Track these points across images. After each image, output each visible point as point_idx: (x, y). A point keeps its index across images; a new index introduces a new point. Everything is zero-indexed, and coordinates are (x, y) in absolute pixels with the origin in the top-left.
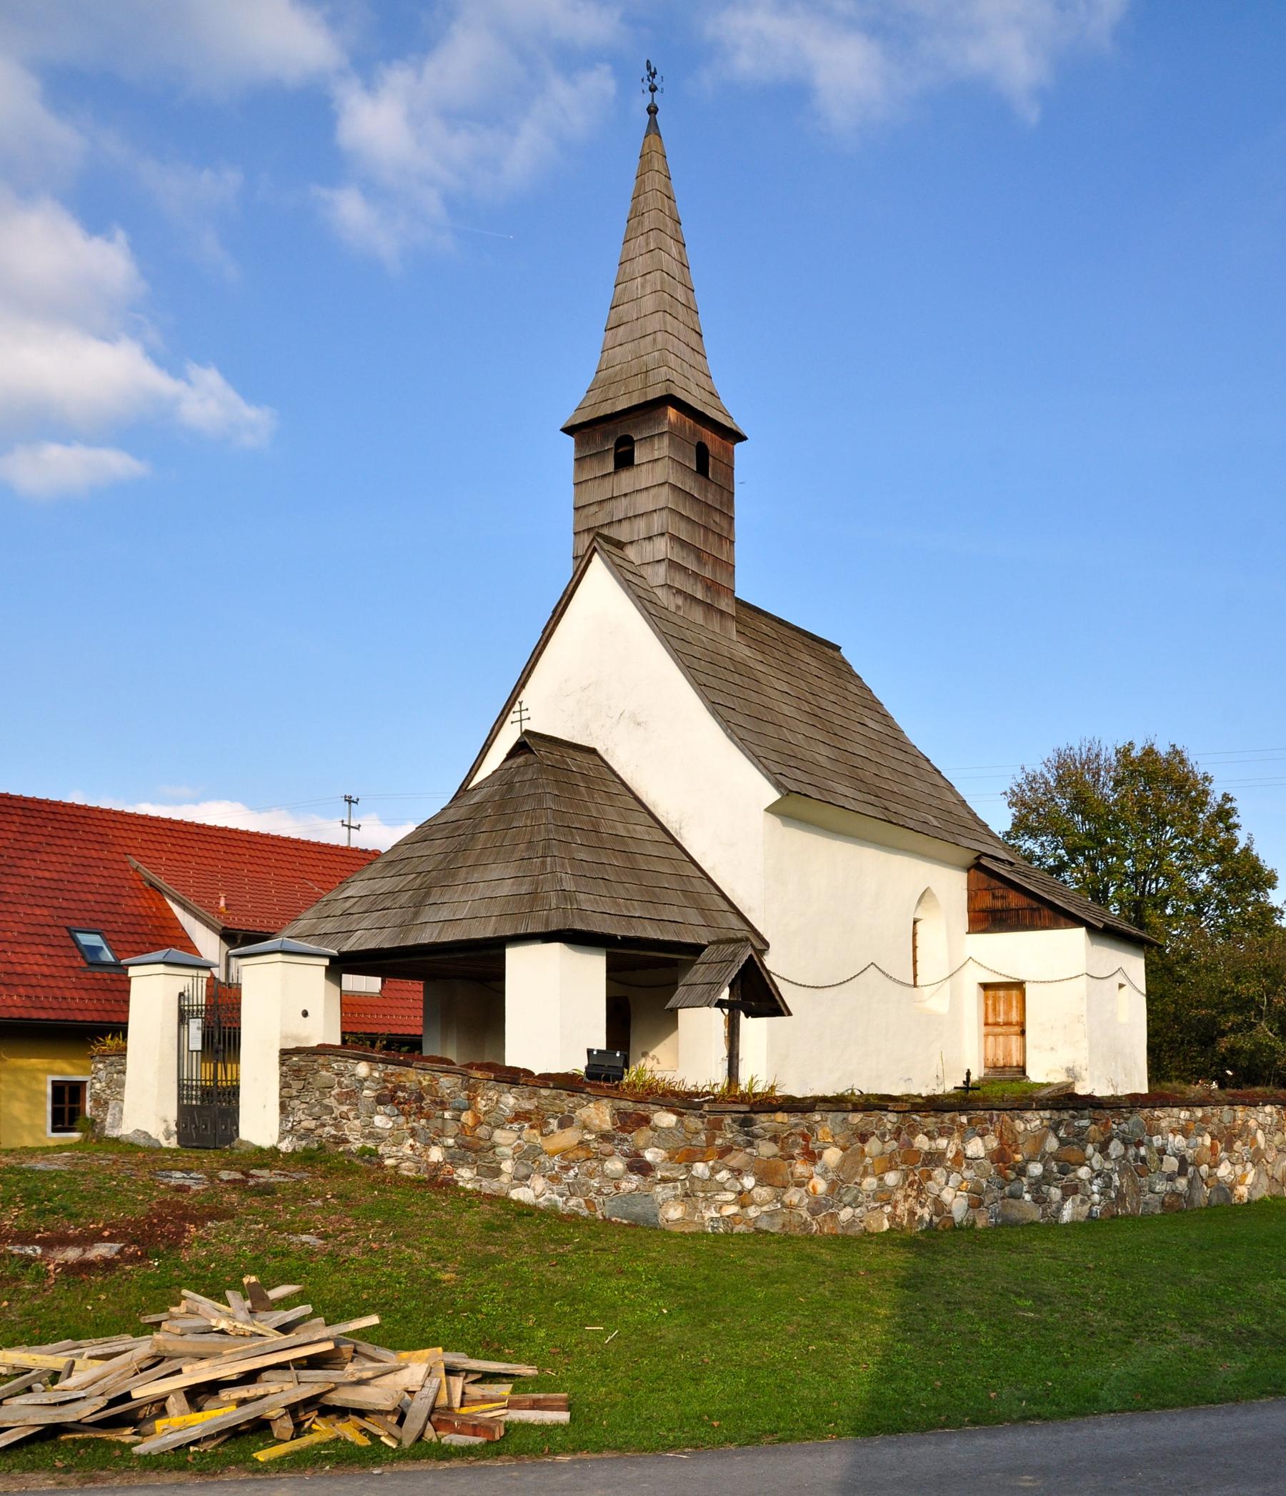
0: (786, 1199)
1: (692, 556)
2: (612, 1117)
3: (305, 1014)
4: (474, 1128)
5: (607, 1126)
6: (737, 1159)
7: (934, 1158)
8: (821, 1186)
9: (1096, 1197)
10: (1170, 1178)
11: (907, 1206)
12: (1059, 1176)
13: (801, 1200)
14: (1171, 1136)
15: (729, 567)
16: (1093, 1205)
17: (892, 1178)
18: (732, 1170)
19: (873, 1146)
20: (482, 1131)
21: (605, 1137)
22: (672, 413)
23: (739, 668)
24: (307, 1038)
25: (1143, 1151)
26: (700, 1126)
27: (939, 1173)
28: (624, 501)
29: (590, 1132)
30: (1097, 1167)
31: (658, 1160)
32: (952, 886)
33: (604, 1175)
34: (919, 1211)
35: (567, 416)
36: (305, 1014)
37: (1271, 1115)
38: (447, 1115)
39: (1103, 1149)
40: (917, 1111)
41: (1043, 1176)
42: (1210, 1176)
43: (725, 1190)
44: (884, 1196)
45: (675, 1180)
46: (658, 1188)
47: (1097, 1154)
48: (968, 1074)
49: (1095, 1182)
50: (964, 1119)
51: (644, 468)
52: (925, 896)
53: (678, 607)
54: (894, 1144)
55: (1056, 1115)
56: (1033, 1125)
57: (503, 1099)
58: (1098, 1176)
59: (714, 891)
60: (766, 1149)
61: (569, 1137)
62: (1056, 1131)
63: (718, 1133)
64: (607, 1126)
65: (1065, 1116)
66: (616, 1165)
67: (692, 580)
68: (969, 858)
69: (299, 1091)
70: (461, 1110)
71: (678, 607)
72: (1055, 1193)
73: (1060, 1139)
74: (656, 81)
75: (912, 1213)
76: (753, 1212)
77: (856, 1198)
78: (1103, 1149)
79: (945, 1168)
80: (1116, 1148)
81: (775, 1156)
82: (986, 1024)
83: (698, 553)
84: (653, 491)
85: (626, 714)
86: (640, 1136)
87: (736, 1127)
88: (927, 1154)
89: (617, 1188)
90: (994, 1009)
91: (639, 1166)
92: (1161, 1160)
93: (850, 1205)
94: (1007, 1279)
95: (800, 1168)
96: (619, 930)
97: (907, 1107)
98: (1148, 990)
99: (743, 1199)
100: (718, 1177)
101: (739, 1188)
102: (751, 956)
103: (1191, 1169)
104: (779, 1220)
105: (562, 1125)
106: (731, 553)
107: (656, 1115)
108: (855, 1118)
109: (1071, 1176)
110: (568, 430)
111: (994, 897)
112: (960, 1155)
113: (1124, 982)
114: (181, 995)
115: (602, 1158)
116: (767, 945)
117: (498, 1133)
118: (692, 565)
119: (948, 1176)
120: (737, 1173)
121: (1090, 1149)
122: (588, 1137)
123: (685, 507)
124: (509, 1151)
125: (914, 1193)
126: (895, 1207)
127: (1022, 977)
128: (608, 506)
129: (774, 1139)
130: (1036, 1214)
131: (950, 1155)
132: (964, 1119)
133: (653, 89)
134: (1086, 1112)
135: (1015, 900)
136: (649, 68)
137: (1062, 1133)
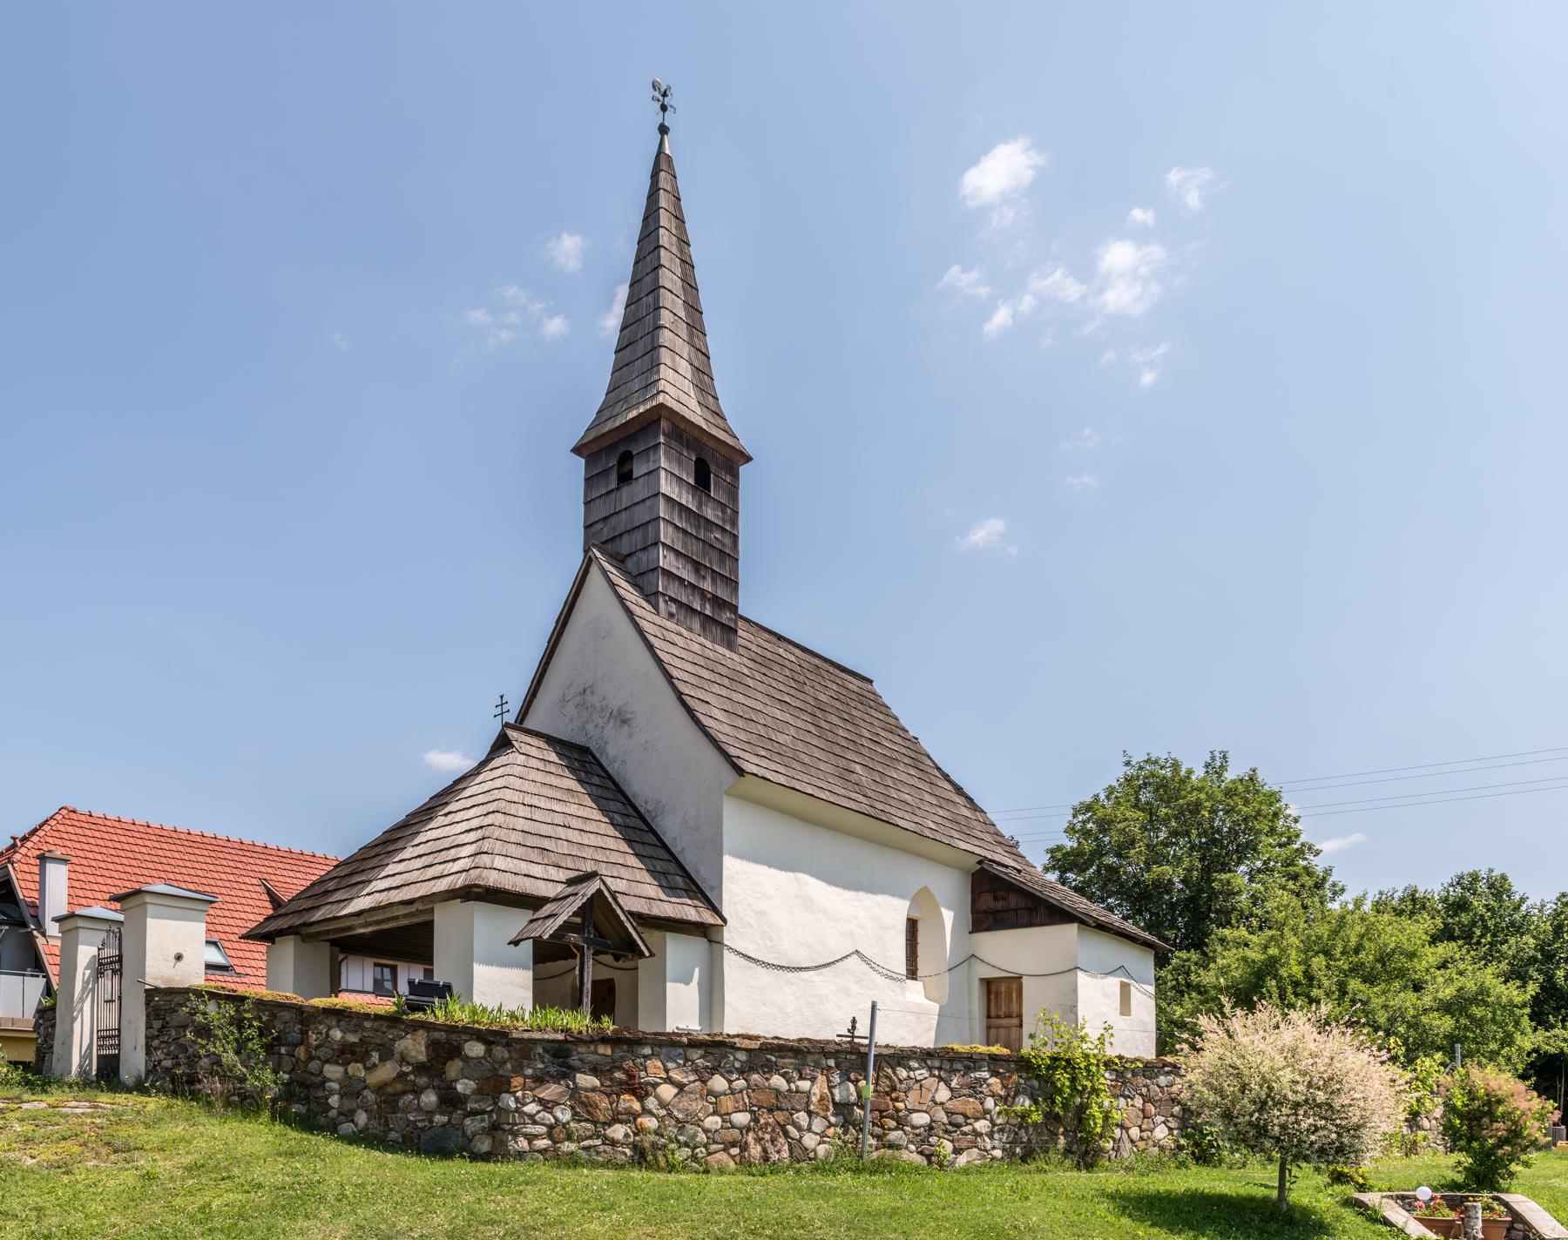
1: (689, 567)
2: (427, 1047)
3: (179, 957)
4: (306, 1063)
5: (423, 1058)
13: (627, 1135)
15: (733, 584)
18: (541, 1101)
20: (314, 1066)
26: (507, 1055)
28: (624, 515)
29: (408, 1064)
31: (468, 1092)
33: (419, 1109)
36: (179, 957)
38: (283, 1050)
42: (1142, 1139)
43: (535, 1123)
45: (483, 1112)
46: (468, 1121)
48: (854, 1021)
57: (332, 1033)
61: (386, 1072)
63: (526, 1062)
64: (423, 1058)
66: (429, 1098)
69: (160, 1030)
70: (296, 1045)
82: (989, 1017)
83: (697, 566)
84: (648, 503)
87: (547, 1057)
89: (431, 1121)
91: (451, 1100)
93: (686, 1145)
100: (526, 1109)
105: (382, 1059)
106: (735, 570)
107: (467, 1046)
110: (577, 450)
111: (996, 899)
115: (417, 1092)
116: (725, 921)
117: (327, 1067)
118: (686, 574)
120: (547, 1105)
122: (405, 1069)
124: (335, 1086)
125: (768, 1137)
127: (1021, 971)
128: (614, 520)
135: (1013, 901)
136: (655, 86)
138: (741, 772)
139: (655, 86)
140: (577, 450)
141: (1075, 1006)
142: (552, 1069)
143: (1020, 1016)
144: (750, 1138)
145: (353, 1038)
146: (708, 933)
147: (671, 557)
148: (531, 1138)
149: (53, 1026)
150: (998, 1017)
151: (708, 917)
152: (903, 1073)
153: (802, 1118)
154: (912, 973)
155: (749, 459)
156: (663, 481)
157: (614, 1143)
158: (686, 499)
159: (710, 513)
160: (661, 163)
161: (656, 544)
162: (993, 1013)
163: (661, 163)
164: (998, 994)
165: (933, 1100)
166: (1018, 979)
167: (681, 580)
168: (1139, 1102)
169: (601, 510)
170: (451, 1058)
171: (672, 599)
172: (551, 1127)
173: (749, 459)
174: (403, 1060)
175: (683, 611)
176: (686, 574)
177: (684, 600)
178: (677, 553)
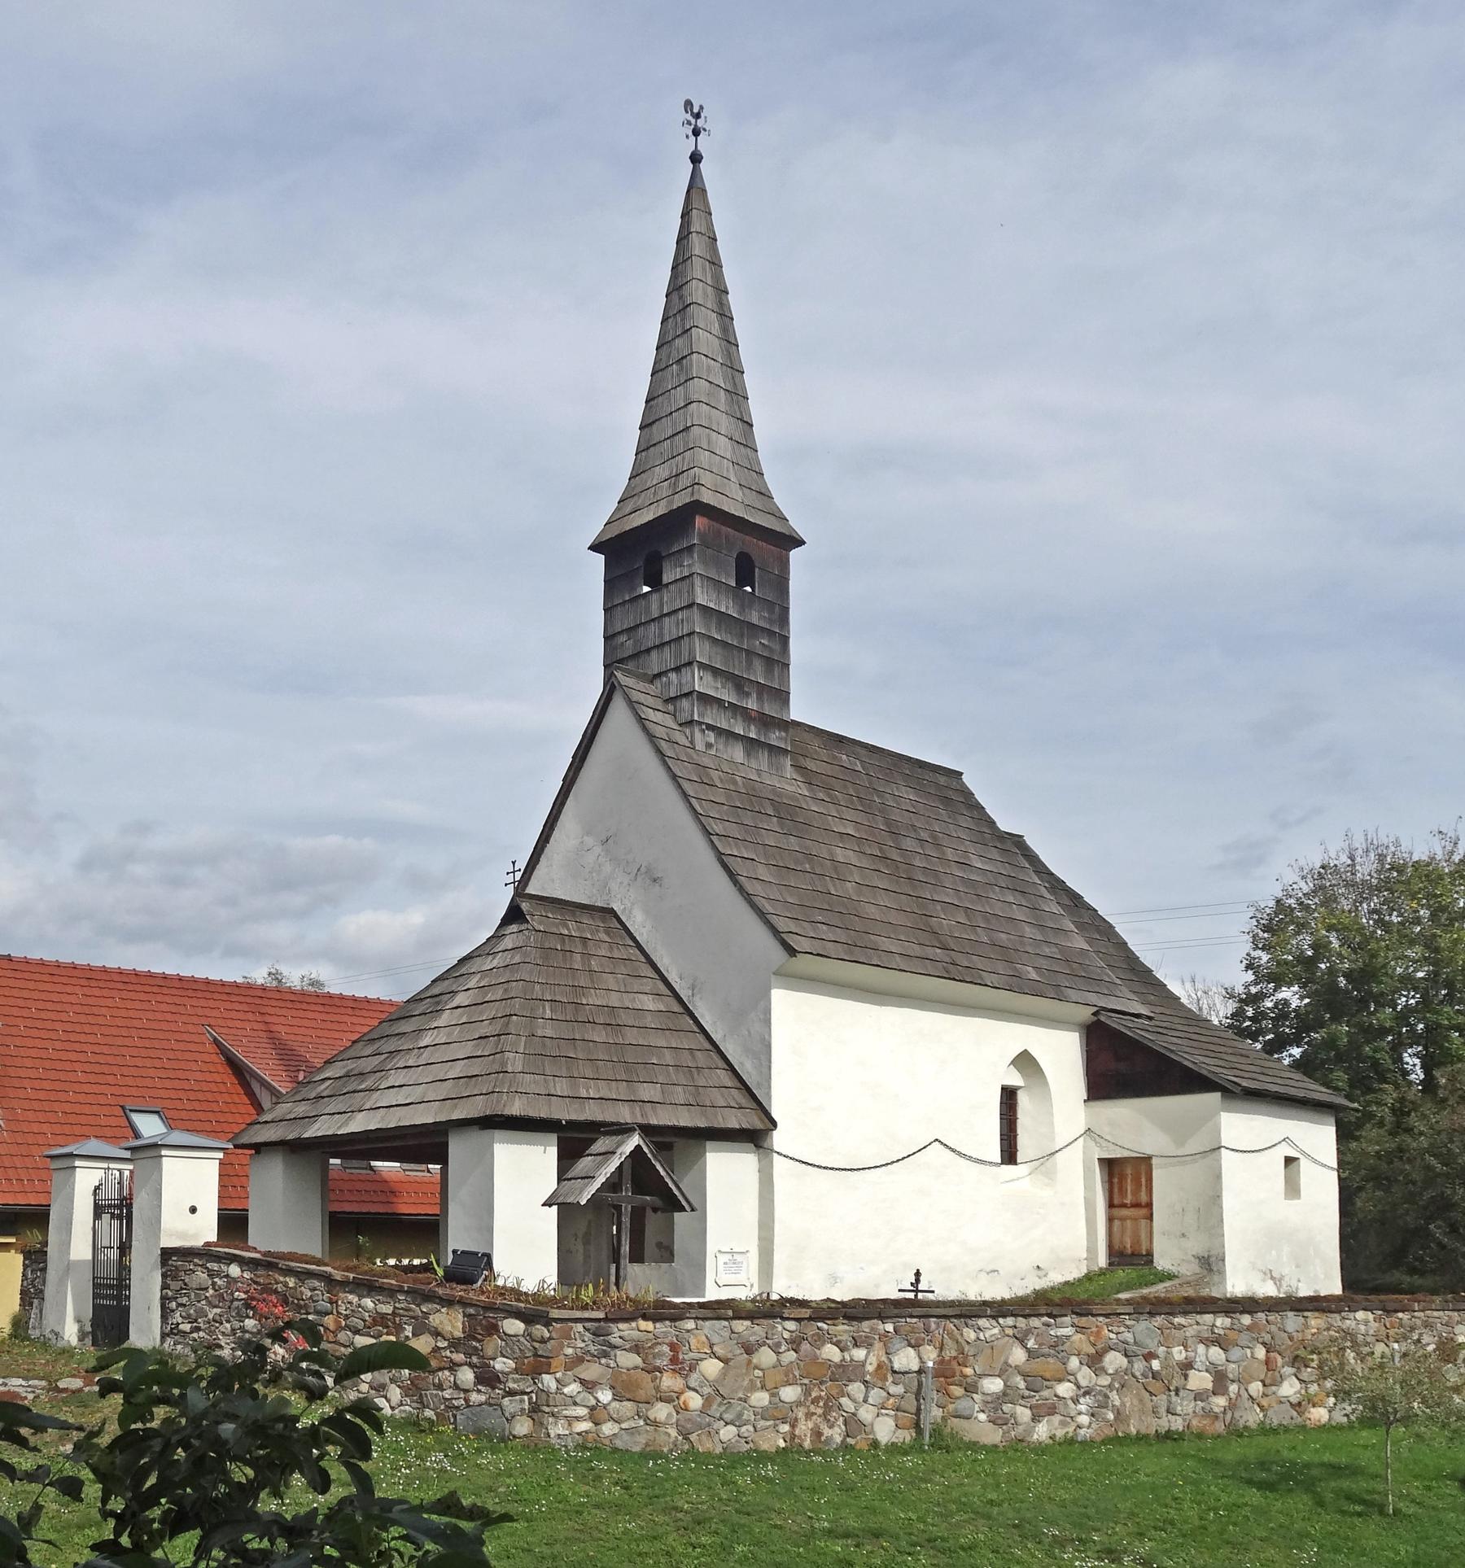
0: (652, 1415)
3: (193, 1210)
5: (459, 1334)
6: (591, 1371)
7: (846, 1372)
8: (695, 1401)
9: (1084, 1419)
10: (1199, 1396)
11: (810, 1425)
12: (1027, 1393)
13: (669, 1415)
14: (1201, 1348)
16: (1079, 1427)
17: (790, 1394)
18: (583, 1382)
19: (766, 1357)
21: (455, 1344)
22: (700, 522)
23: (786, 812)
24: (195, 1236)
25: (1156, 1364)
27: (856, 1389)
28: (653, 627)
30: (1083, 1383)
32: (1062, 1053)
33: (456, 1387)
34: (827, 1432)
35: (594, 530)
36: (193, 1210)
37: (1366, 1322)
39: (1094, 1361)
40: (822, 1320)
41: (1005, 1394)
42: (1265, 1395)
43: (575, 1404)
44: (778, 1413)
47: (1085, 1369)
48: (918, 1274)
49: (1082, 1400)
50: (890, 1327)
51: (672, 587)
52: (1025, 1061)
53: (709, 746)
54: (791, 1356)
55: (1021, 1322)
56: (988, 1334)
58: (1086, 1394)
59: (721, 1064)
60: (628, 1360)
62: (1022, 1342)
64: (459, 1334)
65: (1035, 1322)
66: (467, 1376)
67: (729, 714)
68: (1085, 1014)
71: (709, 746)
72: (1024, 1414)
73: (1028, 1351)
74: (700, 123)
75: (817, 1434)
76: (608, 1429)
77: (740, 1415)
78: (1094, 1361)
79: (865, 1382)
80: (1114, 1361)
81: (636, 1368)
83: (739, 684)
85: (643, 869)
86: (493, 1344)
88: (838, 1366)
90: (1120, 1189)
91: (487, 1378)
92: (1186, 1377)
93: (732, 1423)
94: (440, 1558)
95: (669, 1382)
96: (564, 1113)
97: (806, 1313)
98: (1340, 1163)
99: (596, 1414)
100: (566, 1390)
101: (593, 1402)
102: (638, 1147)
103: (1233, 1388)
104: (642, 1439)
108: (741, 1326)
109: (1046, 1393)
110: (595, 547)
112: (885, 1371)
113: (1293, 1154)
114: (97, 1188)
115: (453, 1367)
116: (774, 1124)
118: (728, 695)
119: (867, 1392)
120: (589, 1386)
121: (1074, 1362)
122: (440, 1344)
123: (719, 630)
125: (820, 1411)
126: (793, 1426)
127: (1149, 1152)
129: (636, 1349)
130: (993, 1436)
131: (870, 1368)
132: (890, 1327)
133: (696, 133)
134: (1067, 1320)
136: (688, 104)
137: (1031, 1344)
138: (792, 952)
139: (688, 104)
140: (595, 547)
141: (1219, 1197)
142: (592, 1348)
143: (1150, 1205)
144: (801, 1413)
145: (387, 1309)
146: (755, 1135)
147: (708, 677)
148: (571, 1420)
149: (44, 1270)
150: (1124, 1206)
151: (757, 1123)
152: (970, 1334)
153: (856, 1389)
154: (1009, 1155)
155: (801, 543)
156: (698, 590)
157: (655, 1424)
158: (727, 606)
159: (754, 618)
160: (695, 188)
161: (690, 664)
162: (1116, 1202)
163: (695, 188)
164: (1122, 1178)
165: (1006, 1363)
166: (1147, 1160)
167: (720, 702)
168: (1261, 1352)
169: (623, 622)
170: (490, 1335)
171: (710, 727)
172: (592, 1409)
173: (801, 543)
174: (437, 1334)
175: (722, 740)
176: (728, 695)
177: (725, 726)
178: (716, 672)
